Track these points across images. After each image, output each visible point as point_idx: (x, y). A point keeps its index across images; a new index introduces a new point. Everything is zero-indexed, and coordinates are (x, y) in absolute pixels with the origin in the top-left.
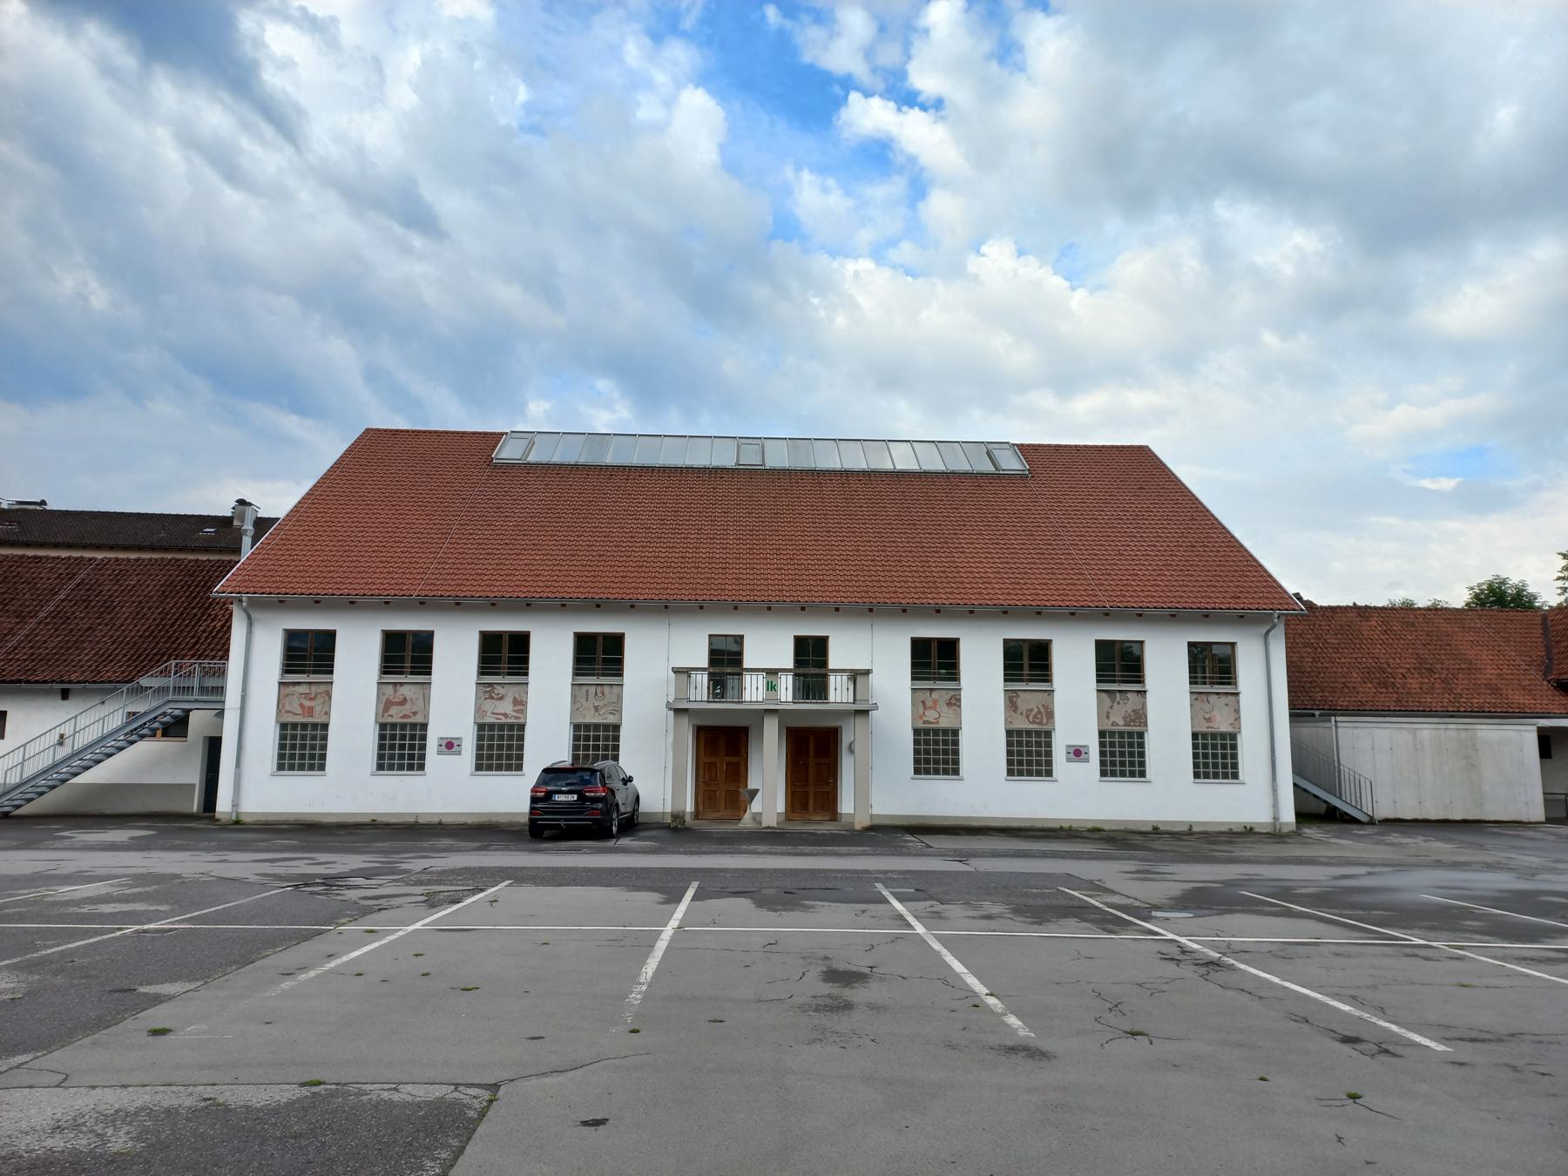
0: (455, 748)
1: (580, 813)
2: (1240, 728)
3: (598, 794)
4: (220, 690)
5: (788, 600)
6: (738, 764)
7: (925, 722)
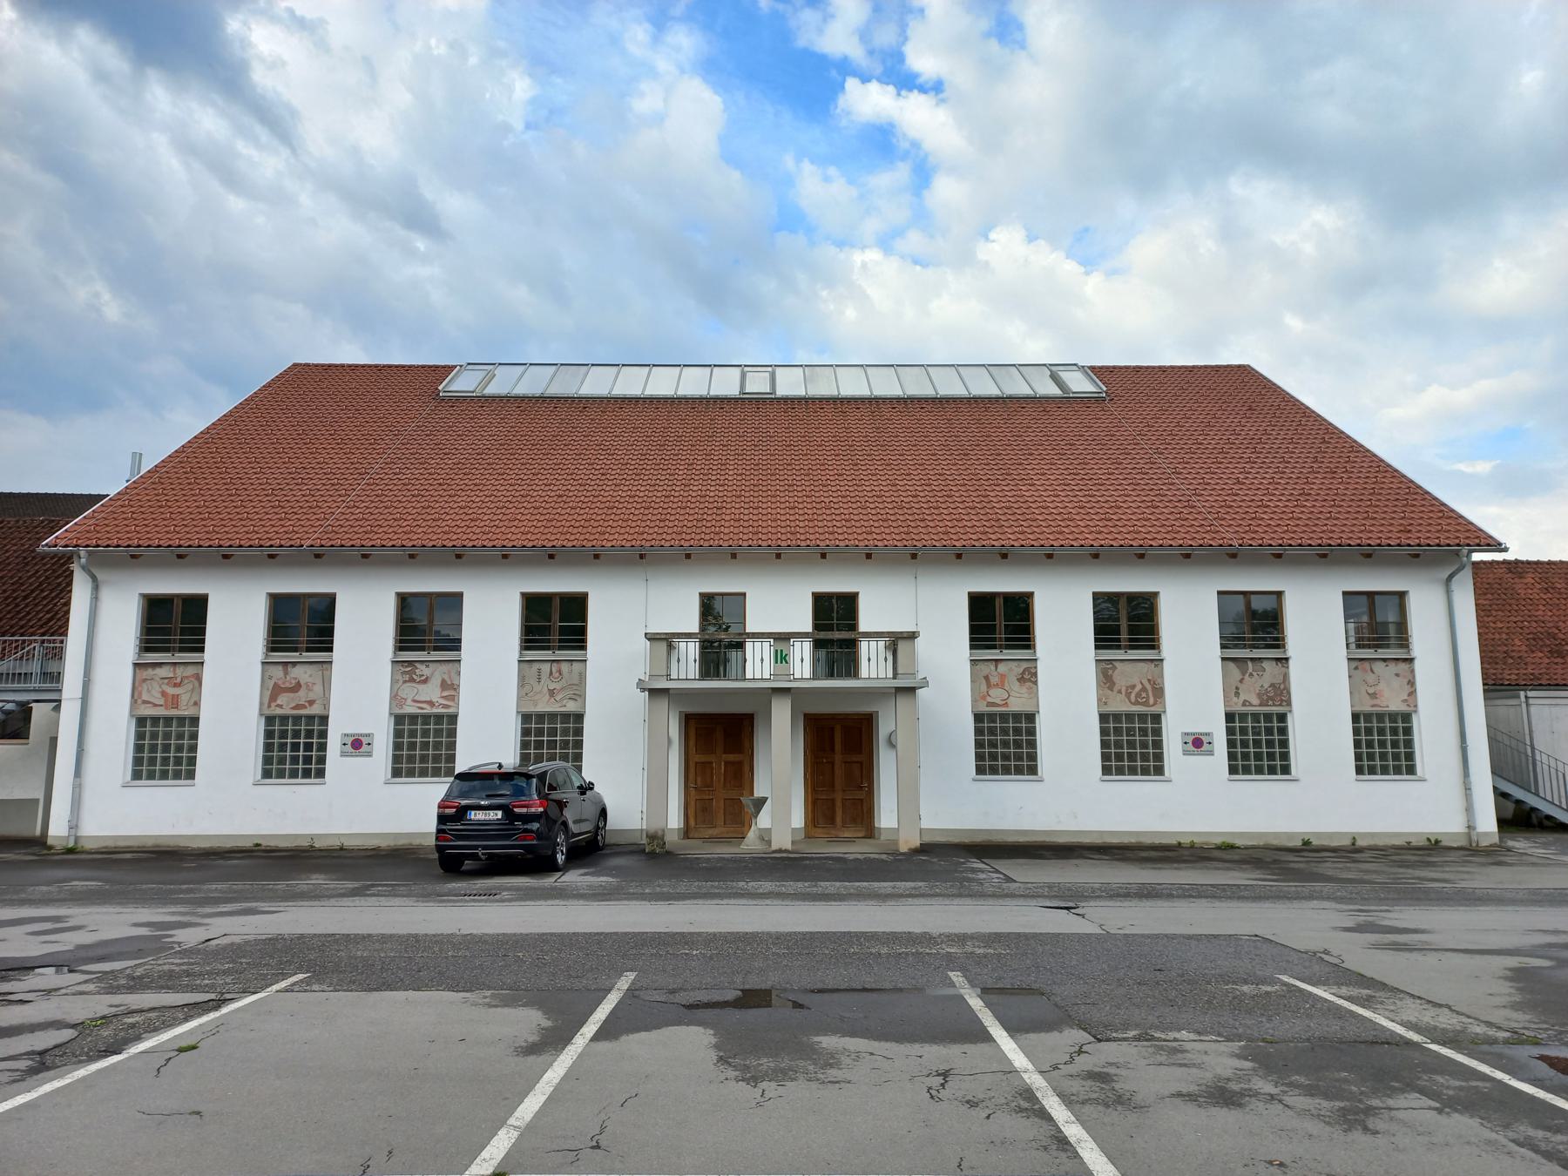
0: (365, 748)
1: (508, 837)
2: (1416, 706)
3: (533, 810)
4: (57, 677)
5: (803, 544)
6: (740, 763)
7: (990, 704)
